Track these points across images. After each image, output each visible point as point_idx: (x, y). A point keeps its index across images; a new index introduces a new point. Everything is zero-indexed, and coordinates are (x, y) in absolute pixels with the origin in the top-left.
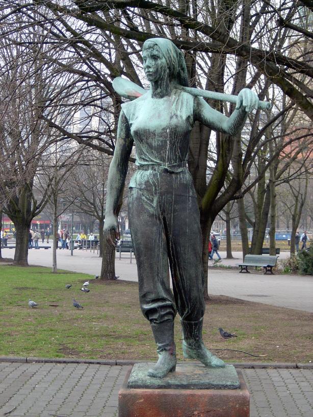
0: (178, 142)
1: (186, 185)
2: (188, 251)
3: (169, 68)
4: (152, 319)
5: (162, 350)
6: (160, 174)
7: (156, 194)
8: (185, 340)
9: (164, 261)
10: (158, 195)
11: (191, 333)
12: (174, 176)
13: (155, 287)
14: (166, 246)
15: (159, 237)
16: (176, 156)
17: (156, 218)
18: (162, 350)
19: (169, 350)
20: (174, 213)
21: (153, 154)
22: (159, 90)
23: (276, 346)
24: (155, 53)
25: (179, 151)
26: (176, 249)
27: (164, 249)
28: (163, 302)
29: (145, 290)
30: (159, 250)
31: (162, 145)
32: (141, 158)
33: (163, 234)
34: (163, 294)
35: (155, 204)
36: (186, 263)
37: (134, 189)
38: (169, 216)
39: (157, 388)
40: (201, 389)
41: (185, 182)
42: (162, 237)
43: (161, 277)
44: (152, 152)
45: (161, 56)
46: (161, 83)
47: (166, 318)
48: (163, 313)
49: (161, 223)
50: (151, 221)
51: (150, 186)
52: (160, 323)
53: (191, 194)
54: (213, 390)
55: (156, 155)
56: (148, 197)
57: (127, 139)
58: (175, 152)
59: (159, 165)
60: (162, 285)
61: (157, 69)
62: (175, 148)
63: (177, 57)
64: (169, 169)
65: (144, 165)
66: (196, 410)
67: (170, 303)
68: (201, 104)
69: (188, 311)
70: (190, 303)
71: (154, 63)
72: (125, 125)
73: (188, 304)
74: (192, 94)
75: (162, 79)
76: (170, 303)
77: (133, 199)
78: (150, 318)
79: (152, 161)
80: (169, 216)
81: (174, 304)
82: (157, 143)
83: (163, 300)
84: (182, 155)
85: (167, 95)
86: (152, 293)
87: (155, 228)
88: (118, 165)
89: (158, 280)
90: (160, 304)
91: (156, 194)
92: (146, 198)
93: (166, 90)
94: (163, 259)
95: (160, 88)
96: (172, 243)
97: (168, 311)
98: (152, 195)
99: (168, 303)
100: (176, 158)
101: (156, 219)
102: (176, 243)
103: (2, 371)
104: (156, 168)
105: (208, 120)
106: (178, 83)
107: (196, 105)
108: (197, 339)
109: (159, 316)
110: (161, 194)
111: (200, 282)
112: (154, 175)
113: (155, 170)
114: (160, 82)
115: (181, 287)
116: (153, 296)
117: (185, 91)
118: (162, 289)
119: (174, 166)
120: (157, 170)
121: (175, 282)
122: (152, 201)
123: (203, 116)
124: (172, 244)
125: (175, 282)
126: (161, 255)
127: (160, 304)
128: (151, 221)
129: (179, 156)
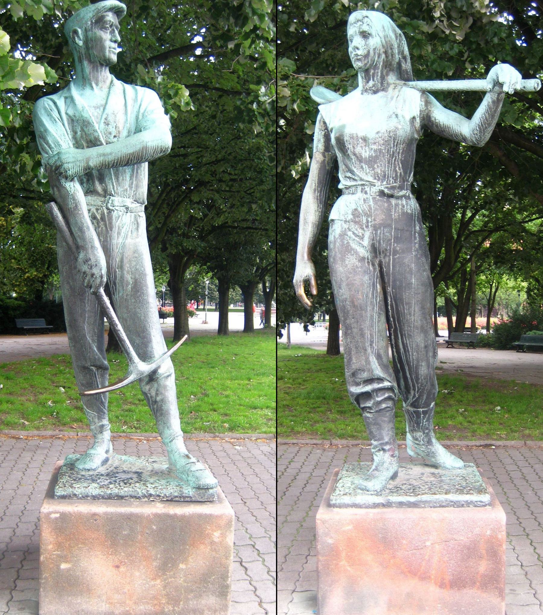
0: (399, 153)
1: (411, 215)
2: (414, 311)
3: (386, 53)
4: (365, 407)
5: (379, 450)
6: (373, 198)
7: (367, 227)
8: (57, 173)
9: (379, 324)
10: (371, 229)
11: (418, 424)
12: (393, 201)
13: (368, 362)
14: (382, 303)
15: (373, 292)
16: (396, 171)
17: (368, 262)
18: (379, 450)
19: (389, 450)
20: (393, 256)
21: (363, 169)
22: (371, 83)
23: (58, 387)
24: (365, 28)
25: (401, 166)
26: (397, 309)
27: (380, 308)
28: (379, 383)
29: (353, 367)
30: (373, 308)
31: (376, 156)
32: (346, 177)
33: (378, 286)
34: (378, 372)
35: (366, 242)
36: (411, 327)
37: (336, 222)
38: (387, 259)
39: (371, 508)
40: (434, 507)
41: (409, 211)
42: (377, 290)
43: (376, 347)
44: (362, 167)
45: (374, 34)
46: (373, 74)
47: (384, 406)
48: (379, 399)
49: (375, 269)
50: (361, 267)
51: (358, 217)
52: (376, 412)
53: (418, 228)
54: (452, 508)
55: (368, 171)
56: (356, 232)
57: (326, 153)
58: (395, 167)
59: (372, 185)
60: (377, 359)
61: (369, 52)
62: (395, 160)
63: (397, 39)
64: (386, 191)
65: (350, 187)
66: (428, 540)
67: (389, 384)
68: (430, 103)
69: (414, 394)
70: (417, 383)
71: (363, 42)
72: (323, 133)
73: (414, 386)
74: (418, 90)
75: (375, 67)
76: (389, 384)
77: (334, 237)
78: (362, 406)
79: (361, 180)
80: (387, 259)
81: (395, 385)
82: (368, 153)
83: (380, 380)
84: (405, 173)
85: (383, 90)
86: (364, 371)
87: (366, 278)
88: (315, 190)
89: (372, 352)
90: (376, 386)
91: (367, 227)
92: (354, 233)
93: (382, 84)
94: (379, 321)
95: (373, 80)
96: (391, 298)
97: (386, 395)
98: (363, 229)
99: (386, 384)
100: (396, 175)
101: (369, 265)
102: (397, 300)
103: (2, 520)
104: (367, 189)
105: (442, 124)
106: (398, 79)
107: (423, 104)
108: (427, 431)
109: (374, 404)
110: (375, 228)
111: (431, 354)
112: (364, 200)
113: (366, 193)
114: (372, 71)
115: (405, 363)
116: (365, 375)
117: (408, 86)
118: (377, 364)
119: (393, 188)
120: (368, 192)
121: (395, 354)
122: (362, 238)
123: (433, 119)
124: (391, 301)
125: (395, 354)
126: (376, 316)
127: (376, 386)
128: (361, 267)
129: (401, 173)
